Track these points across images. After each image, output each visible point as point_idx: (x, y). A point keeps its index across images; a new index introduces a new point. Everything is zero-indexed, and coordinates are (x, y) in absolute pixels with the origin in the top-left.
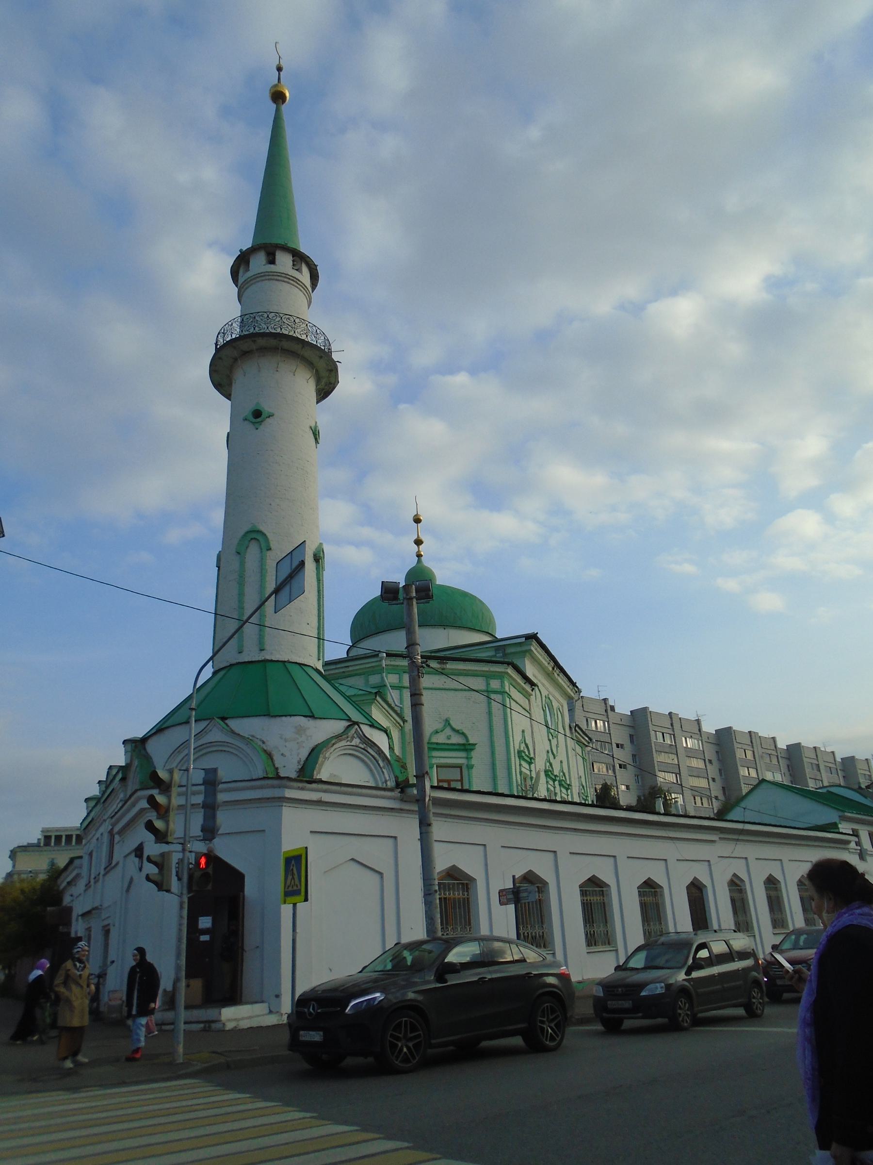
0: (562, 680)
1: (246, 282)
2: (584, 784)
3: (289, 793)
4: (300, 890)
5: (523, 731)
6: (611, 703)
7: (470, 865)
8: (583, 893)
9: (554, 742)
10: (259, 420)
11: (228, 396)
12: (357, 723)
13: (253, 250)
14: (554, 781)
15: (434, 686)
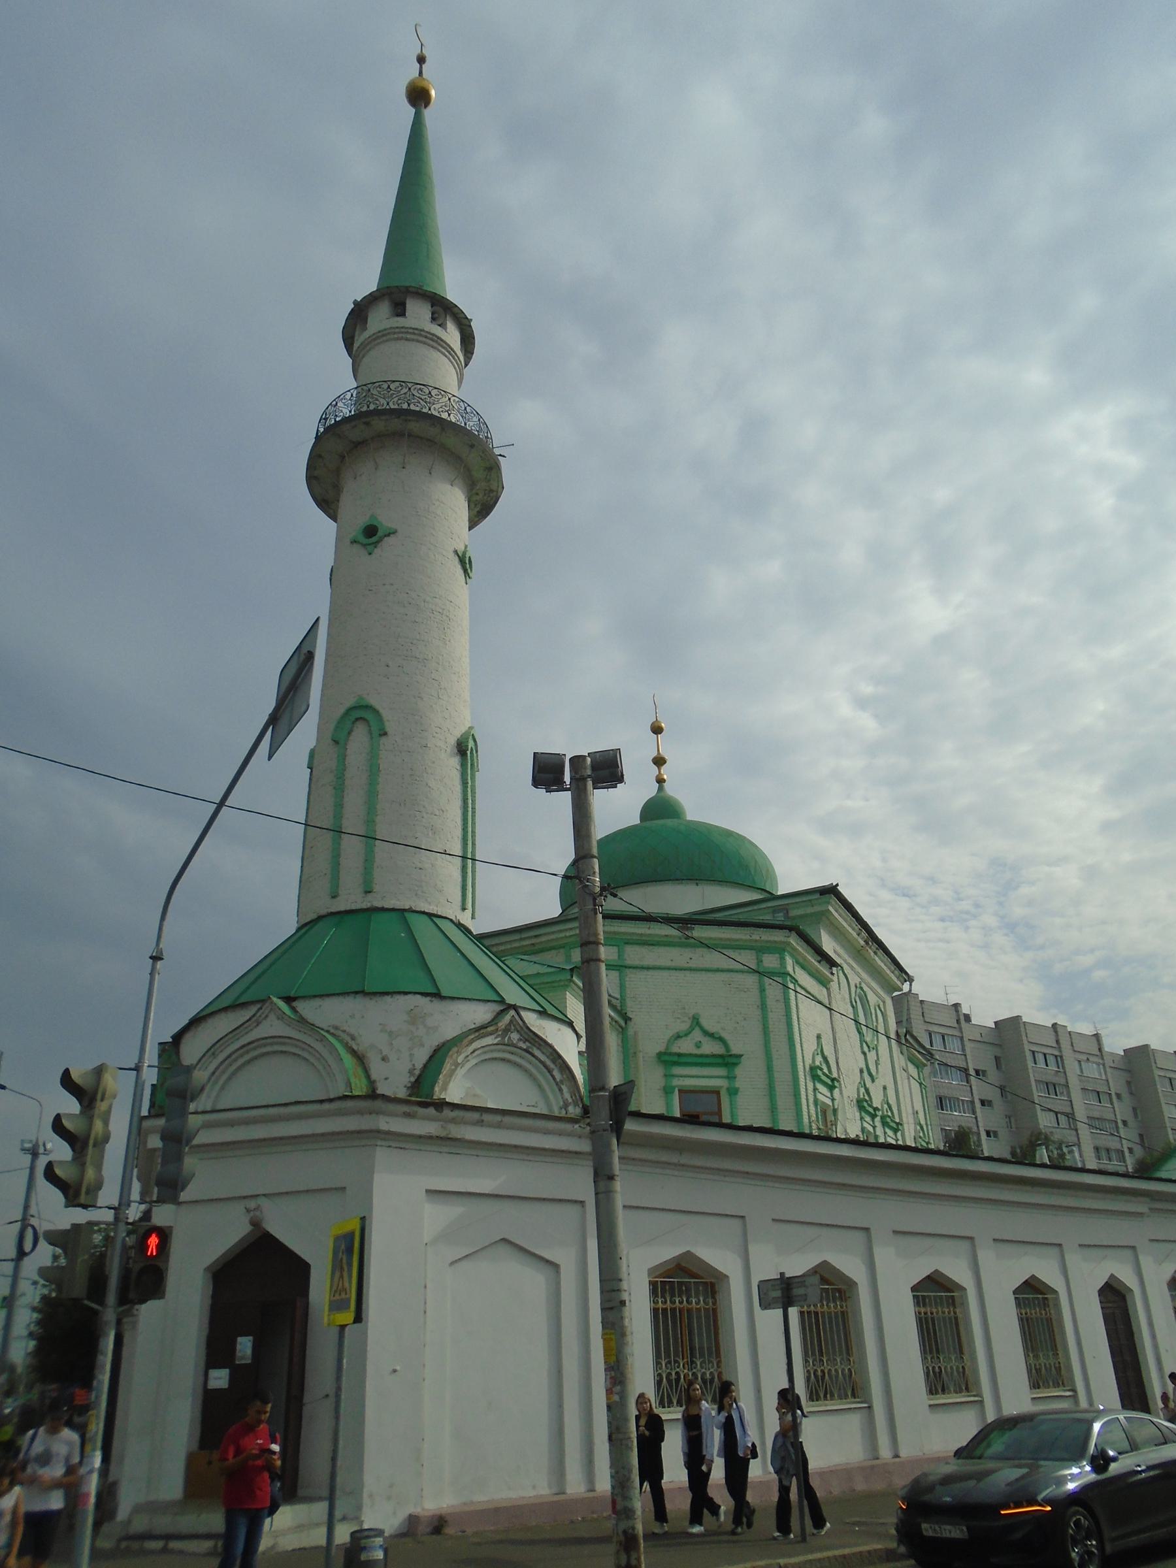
0: (880, 961)
1: (364, 345)
2: (923, 1122)
3: (384, 1123)
4: (349, 1300)
5: (819, 1037)
8: (919, 1301)
9: (871, 1056)
10: (374, 539)
11: (334, 518)
12: (515, 1007)
14: (873, 1116)
15: (673, 964)
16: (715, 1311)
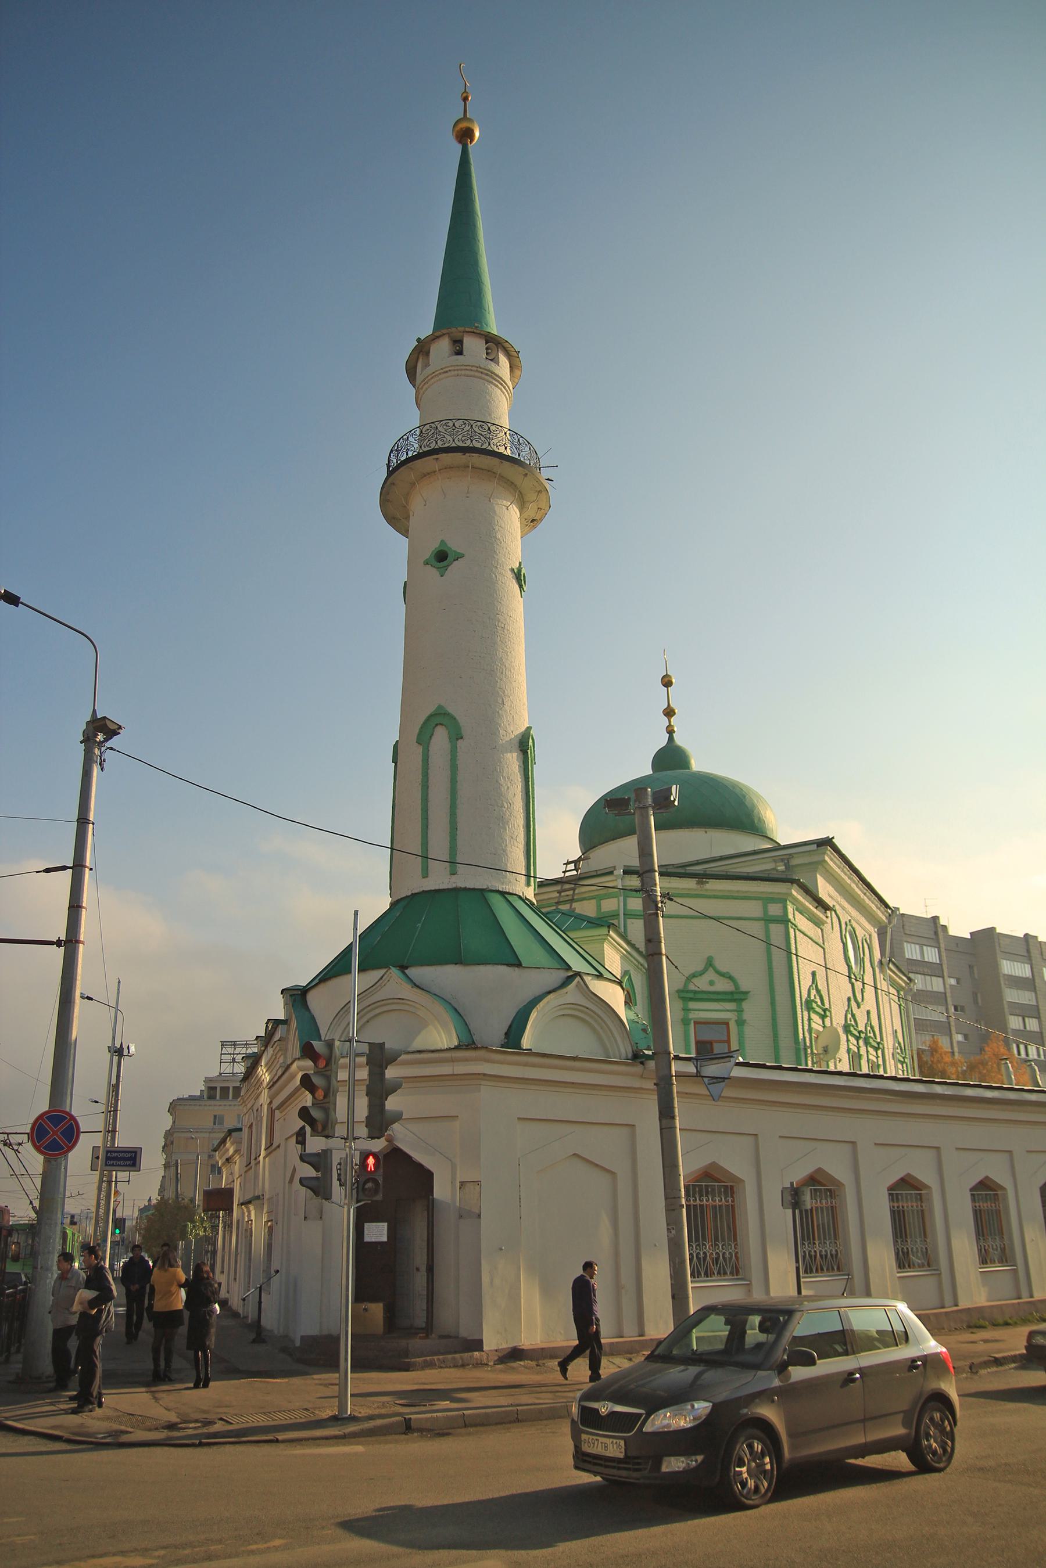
1: (425, 381)
2: (901, 1040)
6: (942, 922)
7: (735, 1163)
9: (858, 985)
10: (445, 563)
11: (405, 532)
12: (578, 974)
13: (434, 338)
16: (733, 1206)
